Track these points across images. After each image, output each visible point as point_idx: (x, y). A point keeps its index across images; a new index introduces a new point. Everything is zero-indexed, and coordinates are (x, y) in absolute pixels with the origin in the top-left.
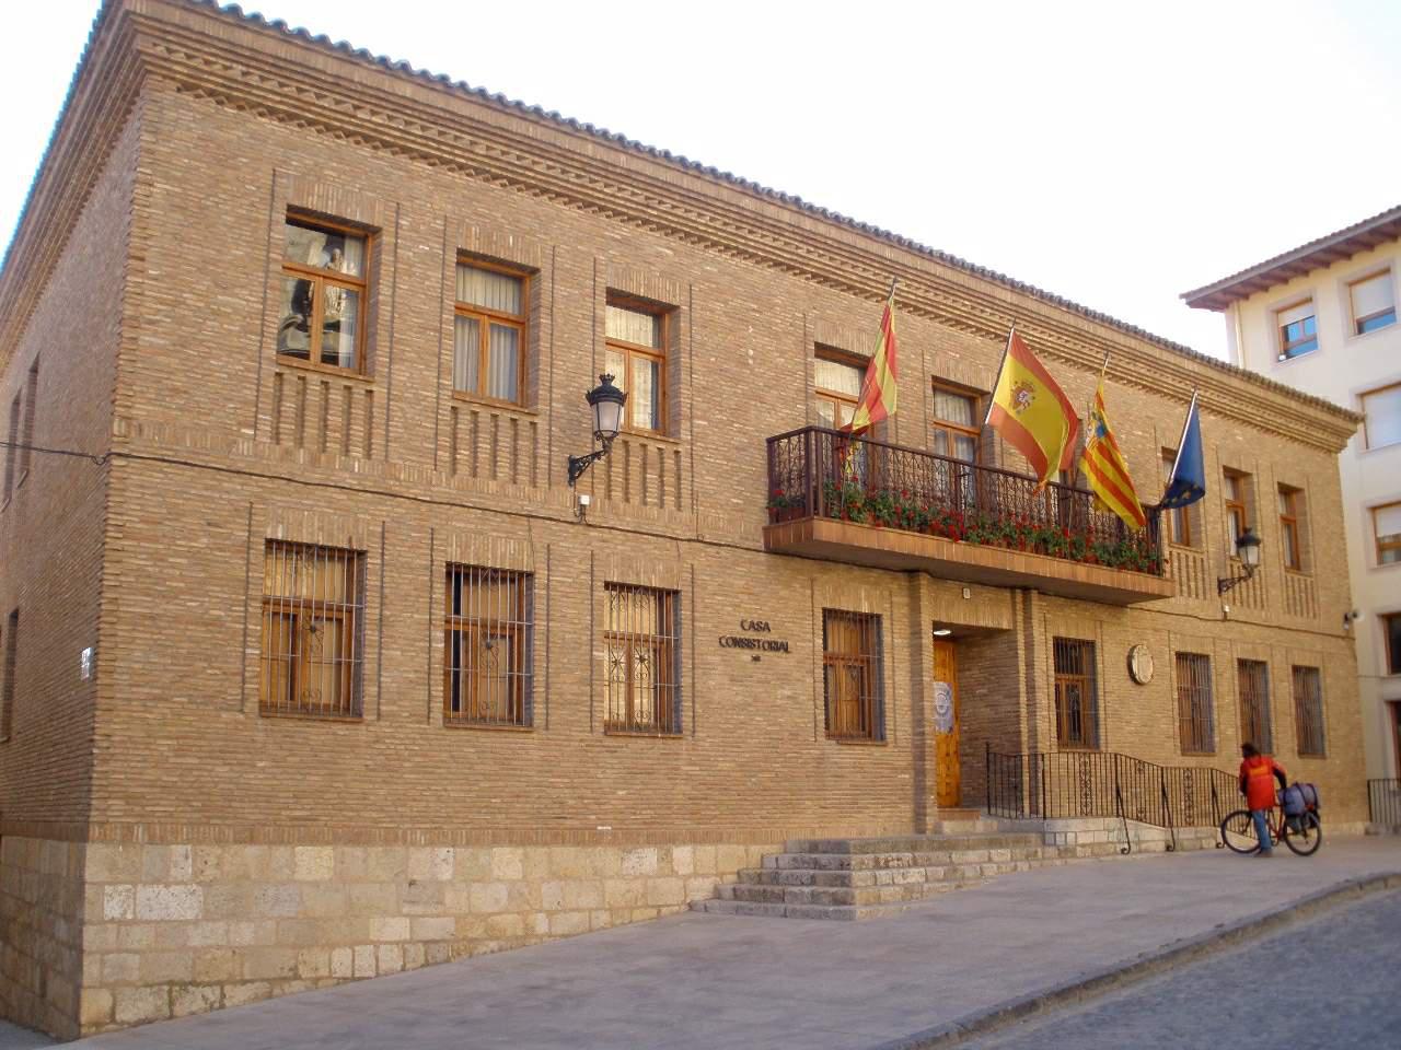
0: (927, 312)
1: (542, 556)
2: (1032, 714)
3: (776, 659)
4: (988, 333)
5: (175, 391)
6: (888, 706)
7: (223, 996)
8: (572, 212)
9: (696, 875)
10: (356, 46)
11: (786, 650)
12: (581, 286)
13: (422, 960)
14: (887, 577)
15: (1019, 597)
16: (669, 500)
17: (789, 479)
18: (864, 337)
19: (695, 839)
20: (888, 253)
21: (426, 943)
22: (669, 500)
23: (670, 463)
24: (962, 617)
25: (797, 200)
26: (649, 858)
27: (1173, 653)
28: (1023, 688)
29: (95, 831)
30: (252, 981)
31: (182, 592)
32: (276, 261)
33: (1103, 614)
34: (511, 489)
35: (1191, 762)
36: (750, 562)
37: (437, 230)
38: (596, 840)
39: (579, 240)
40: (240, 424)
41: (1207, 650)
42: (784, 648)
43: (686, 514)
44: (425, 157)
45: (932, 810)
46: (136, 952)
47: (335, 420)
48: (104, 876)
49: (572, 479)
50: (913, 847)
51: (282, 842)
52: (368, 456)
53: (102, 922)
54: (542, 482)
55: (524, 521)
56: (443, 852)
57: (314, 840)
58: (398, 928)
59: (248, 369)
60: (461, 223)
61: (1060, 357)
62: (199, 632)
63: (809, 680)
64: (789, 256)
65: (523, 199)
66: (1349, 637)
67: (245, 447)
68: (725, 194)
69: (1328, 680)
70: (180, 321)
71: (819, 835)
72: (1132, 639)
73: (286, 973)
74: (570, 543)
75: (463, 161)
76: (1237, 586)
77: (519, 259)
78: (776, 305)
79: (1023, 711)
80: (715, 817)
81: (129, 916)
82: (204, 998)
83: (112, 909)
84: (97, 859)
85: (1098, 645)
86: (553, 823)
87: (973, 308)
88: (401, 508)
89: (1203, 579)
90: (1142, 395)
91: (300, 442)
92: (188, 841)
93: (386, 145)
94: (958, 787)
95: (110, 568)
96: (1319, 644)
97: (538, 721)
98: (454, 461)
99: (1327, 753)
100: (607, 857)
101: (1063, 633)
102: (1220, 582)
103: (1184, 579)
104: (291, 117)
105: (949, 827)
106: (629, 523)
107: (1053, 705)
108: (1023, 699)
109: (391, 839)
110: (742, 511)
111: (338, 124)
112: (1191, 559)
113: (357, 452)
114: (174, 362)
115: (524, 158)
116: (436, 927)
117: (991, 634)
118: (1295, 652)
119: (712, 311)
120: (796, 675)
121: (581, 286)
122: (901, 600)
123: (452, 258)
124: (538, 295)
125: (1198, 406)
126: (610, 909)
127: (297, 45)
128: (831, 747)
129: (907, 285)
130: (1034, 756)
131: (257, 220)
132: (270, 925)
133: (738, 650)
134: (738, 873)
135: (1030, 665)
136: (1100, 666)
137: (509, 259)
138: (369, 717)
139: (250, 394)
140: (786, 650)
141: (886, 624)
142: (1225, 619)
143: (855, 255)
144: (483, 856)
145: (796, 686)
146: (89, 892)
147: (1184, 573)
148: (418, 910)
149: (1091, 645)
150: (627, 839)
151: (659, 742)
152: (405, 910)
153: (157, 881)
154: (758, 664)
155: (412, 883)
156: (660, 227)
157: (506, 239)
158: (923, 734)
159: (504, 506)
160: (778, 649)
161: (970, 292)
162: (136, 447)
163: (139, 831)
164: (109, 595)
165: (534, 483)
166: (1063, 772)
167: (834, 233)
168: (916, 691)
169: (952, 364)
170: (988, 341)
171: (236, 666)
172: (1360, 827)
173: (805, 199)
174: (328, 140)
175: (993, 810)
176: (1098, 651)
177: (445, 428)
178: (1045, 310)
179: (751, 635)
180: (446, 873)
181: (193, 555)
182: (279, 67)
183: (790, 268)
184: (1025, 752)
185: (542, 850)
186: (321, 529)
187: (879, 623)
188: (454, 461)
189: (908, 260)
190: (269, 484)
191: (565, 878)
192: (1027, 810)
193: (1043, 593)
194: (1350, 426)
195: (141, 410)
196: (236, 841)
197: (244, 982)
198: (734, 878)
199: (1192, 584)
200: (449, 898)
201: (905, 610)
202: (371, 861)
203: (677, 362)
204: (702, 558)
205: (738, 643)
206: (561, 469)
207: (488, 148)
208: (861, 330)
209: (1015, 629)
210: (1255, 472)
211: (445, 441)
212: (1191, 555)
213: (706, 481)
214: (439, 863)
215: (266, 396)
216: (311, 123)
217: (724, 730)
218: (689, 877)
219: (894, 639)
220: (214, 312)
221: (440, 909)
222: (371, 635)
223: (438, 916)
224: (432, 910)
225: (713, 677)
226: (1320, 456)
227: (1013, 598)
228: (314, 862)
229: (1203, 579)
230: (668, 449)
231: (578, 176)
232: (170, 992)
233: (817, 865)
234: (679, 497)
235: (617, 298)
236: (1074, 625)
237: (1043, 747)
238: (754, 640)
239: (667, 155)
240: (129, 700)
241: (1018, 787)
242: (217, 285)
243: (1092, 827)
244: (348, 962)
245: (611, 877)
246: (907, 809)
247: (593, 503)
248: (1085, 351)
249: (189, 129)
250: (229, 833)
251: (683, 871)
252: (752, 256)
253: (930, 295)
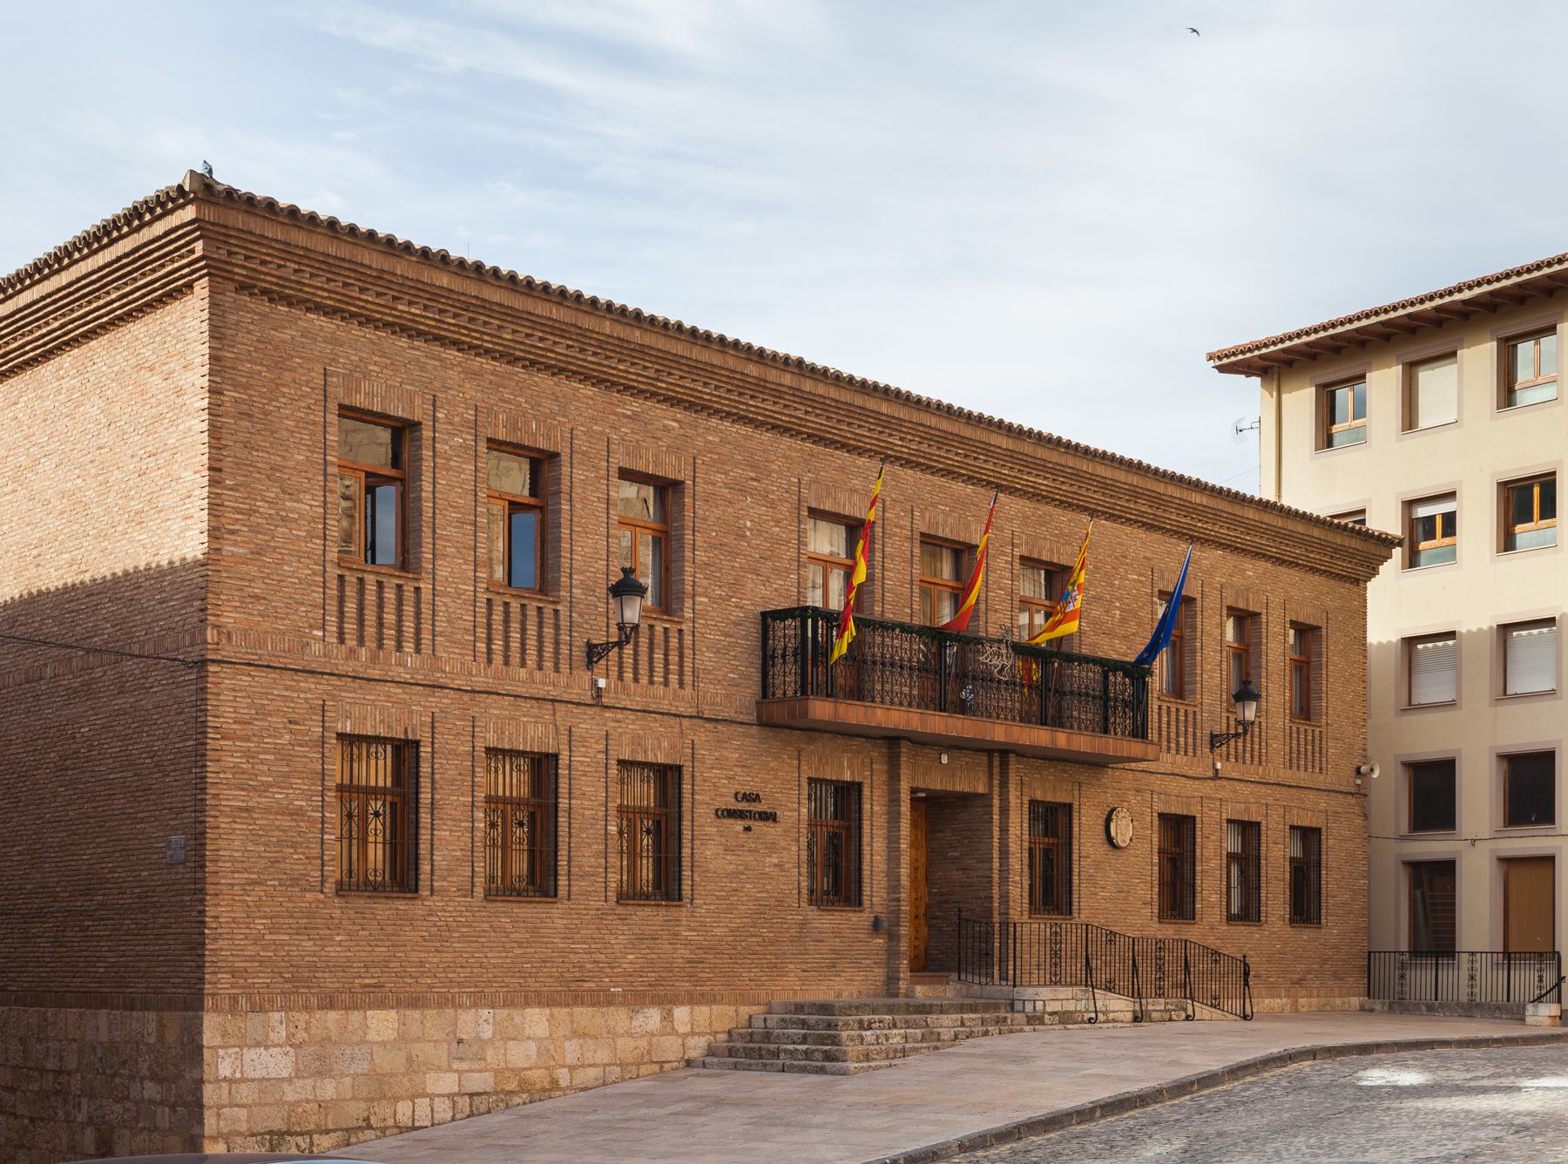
0: (918, 464)
1: (564, 738)
2: (1004, 880)
4: (980, 480)
5: (256, 597)
6: (866, 873)
7: (312, 1144)
8: (588, 391)
9: (693, 1033)
10: (401, 238)
11: (775, 820)
12: (596, 468)
13: (467, 1111)
16: (673, 678)
17: (784, 656)
18: (856, 498)
19: (692, 1000)
20: (884, 408)
21: (471, 1095)
22: (673, 678)
23: (674, 642)
24: (937, 783)
25: (800, 362)
26: (652, 1018)
28: (996, 854)
29: (208, 1002)
30: (334, 1131)
31: (270, 785)
32: (333, 464)
34: (538, 675)
35: (1169, 931)
36: (745, 735)
37: (468, 421)
38: (610, 1001)
39: (594, 420)
40: (311, 627)
41: (1194, 810)
43: (688, 690)
44: (456, 344)
45: (904, 974)
46: (244, 1106)
47: (390, 617)
48: (218, 1041)
49: (590, 664)
50: (890, 1010)
51: (356, 1008)
52: (418, 651)
53: (217, 1081)
54: (564, 667)
55: (549, 706)
56: (485, 1013)
57: (381, 1004)
58: (449, 1083)
59: (314, 574)
60: (490, 411)
61: (1054, 500)
62: (286, 822)
63: (794, 848)
65: (544, 381)
66: (1361, 794)
67: (317, 648)
68: (731, 363)
69: (1331, 842)
70: (255, 529)
71: (799, 999)
72: (1111, 800)
73: (360, 1123)
74: (588, 725)
76: (1232, 742)
77: (542, 444)
78: (774, 471)
79: (996, 876)
80: (710, 979)
81: (238, 1075)
82: (298, 1146)
83: (225, 1070)
84: (212, 1026)
85: (1076, 806)
86: (573, 986)
87: (966, 456)
88: (446, 699)
89: (1194, 735)
90: (1141, 534)
91: (361, 641)
92: (282, 1009)
93: (420, 334)
94: (926, 949)
95: (211, 767)
96: (1323, 802)
97: (562, 891)
98: (489, 651)
99: (1323, 921)
100: (618, 1017)
101: (1039, 796)
102: (1213, 737)
103: (1173, 735)
104: (336, 311)
105: (921, 991)
106: (637, 702)
107: (1026, 869)
108: (996, 865)
109: (444, 1002)
110: (737, 685)
112: (1182, 712)
113: (409, 647)
114: (253, 570)
116: (481, 1081)
117: (966, 799)
118: (1295, 811)
119: (714, 484)
120: (783, 844)
121: (596, 468)
124: (558, 481)
126: (621, 1065)
128: (812, 913)
129: (901, 439)
130: (1005, 924)
131: (314, 423)
132: (348, 1080)
133: (732, 821)
134: (729, 1032)
135: (1004, 830)
136: (1076, 829)
137: (531, 444)
138: (425, 893)
139: (318, 597)
140: (775, 820)
141: (866, 792)
142: (1216, 776)
143: (852, 412)
144: (517, 1015)
145: (784, 854)
146: (207, 1054)
147: (1173, 728)
148: (465, 1066)
149: (1069, 808)
150: (636, 1000)
151: (662, 911)
152: (455, 1066)
153: (258, 1045)
154: (750, 834)
155: (460, 1042)
156: (666, 399)
157: (528, 424)
158: (898, 900)
159: (533, 692)
160: (767, 819)
161: (963, 440)
162: (226, 652)
163: (242, 1001)
164: (211, 791)
165: (557, 670)
166: (1035, 938)
167: (833, 393)
168: (886, 851)
169: (941, 518)
170: (980, 490)
171: (316, 851)
172: (1355, 1001)
173: (808, 360)
174: (369, 333)
175: (963, 977)
176: (1075, 814)
177: (482, 620)
178: (1041, 453)
179: (743, 806)
180: (487, 1032)
181: (277, 750)
182: (328, 264)
183: (787, 430)
184: (996, 918)
185: (565, 1010)
186: (382, 721)
187: (860, 790)
188: (489, 651)
189: (903, 413)
190: (335, 681)
191: (584, 1035)
192: (996, 976)
194: (1381, 551)
195: (229, 619)
196: (320, 1008)
197: (327, 1132)
198: (723, 1037)
199: (1182, 740)
200: (490, 1054)
201: (884, 777)
202: (431, 1022)
203: (681, 537)
204: (701, 735)
205: (732, 814)
206: (579, 654)
207: (514, 332)
208: (853, 490)
209: (991, 793)
211: (482, 632)
212: (1310, 729)
213: (706, 658)
214: (479, 1022)
215: (331, 598)
216: (353, 315)
217: (718, 898)
218: (686, 1035)
219: (873, 807)
220: (283, 519)
221: (483, 1065)
222: (425, 818)
223: (480, 1071)
224: (476, 1066)
225: (710, 847)
226: (1343, 588)
228: (382, 1023)
229: (1194, 735)
230: (673, 628)
231: (595, 354)
232: (271, 1141)
233: (804, 1024)
234: (681, 674)
235: (626, 474)
236: (1051, 791)
237: (1014, 915)
238: (748, 811)
239: (679, 326)
240: (233, 885)
241: (988, 954)
242: (284, 492)
243: (1061, 996)
244: (409, 1113)
245: (622, 1036)
246: (879, 973)
247: (608, 685)
248: (1083, 492)
249: (249, 332)
250: (314, 1001)
251: (682, 1029)
252: (751, 421)
253: (924, 447)
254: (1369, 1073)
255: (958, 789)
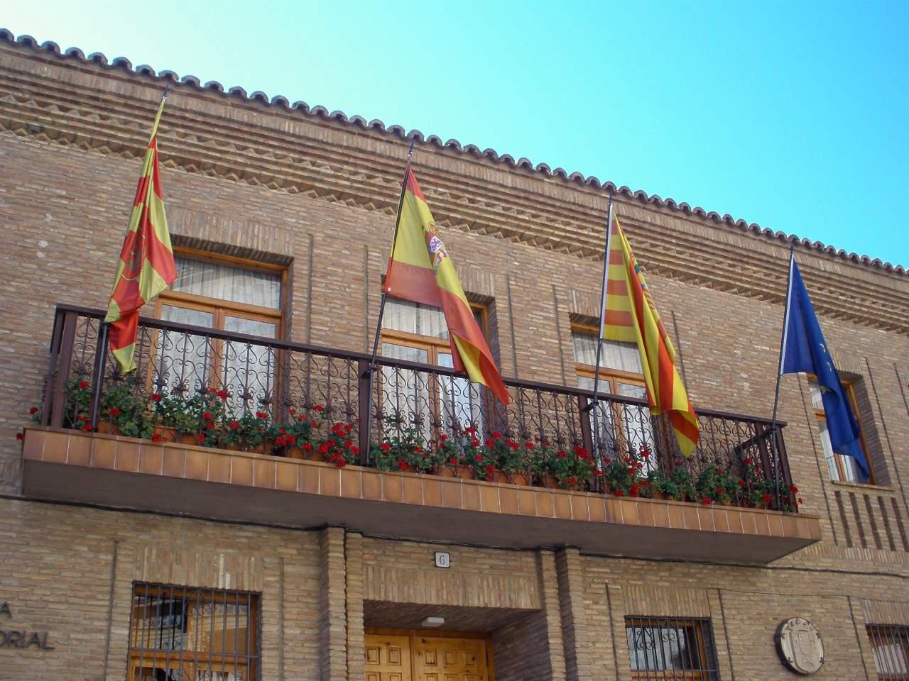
3: (19, 661)
14: (275, 538)
15: (548, 560)
27: (861, 627)
33: (723, 579)
42: (39, 642)
64: (127, 136)
75: (382, 199)
85: (716, 621)
103: (866, 526)
111: (445, 213)
115: (303, 160)
122: (300, 570)
123: (566, 324)
125: (158, 158)
127: (447, 156)
136: (722, 653)
176: (718, 634)
193: (592, 553)
210: (865, 374)
219: (285, 627)
227: (539, 564)
254: (78, 354)
255: (475, 602)
